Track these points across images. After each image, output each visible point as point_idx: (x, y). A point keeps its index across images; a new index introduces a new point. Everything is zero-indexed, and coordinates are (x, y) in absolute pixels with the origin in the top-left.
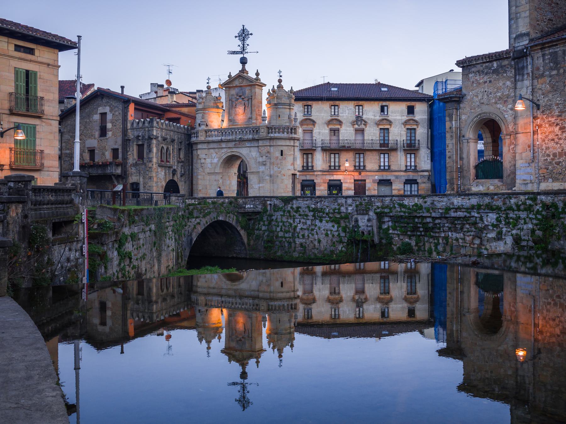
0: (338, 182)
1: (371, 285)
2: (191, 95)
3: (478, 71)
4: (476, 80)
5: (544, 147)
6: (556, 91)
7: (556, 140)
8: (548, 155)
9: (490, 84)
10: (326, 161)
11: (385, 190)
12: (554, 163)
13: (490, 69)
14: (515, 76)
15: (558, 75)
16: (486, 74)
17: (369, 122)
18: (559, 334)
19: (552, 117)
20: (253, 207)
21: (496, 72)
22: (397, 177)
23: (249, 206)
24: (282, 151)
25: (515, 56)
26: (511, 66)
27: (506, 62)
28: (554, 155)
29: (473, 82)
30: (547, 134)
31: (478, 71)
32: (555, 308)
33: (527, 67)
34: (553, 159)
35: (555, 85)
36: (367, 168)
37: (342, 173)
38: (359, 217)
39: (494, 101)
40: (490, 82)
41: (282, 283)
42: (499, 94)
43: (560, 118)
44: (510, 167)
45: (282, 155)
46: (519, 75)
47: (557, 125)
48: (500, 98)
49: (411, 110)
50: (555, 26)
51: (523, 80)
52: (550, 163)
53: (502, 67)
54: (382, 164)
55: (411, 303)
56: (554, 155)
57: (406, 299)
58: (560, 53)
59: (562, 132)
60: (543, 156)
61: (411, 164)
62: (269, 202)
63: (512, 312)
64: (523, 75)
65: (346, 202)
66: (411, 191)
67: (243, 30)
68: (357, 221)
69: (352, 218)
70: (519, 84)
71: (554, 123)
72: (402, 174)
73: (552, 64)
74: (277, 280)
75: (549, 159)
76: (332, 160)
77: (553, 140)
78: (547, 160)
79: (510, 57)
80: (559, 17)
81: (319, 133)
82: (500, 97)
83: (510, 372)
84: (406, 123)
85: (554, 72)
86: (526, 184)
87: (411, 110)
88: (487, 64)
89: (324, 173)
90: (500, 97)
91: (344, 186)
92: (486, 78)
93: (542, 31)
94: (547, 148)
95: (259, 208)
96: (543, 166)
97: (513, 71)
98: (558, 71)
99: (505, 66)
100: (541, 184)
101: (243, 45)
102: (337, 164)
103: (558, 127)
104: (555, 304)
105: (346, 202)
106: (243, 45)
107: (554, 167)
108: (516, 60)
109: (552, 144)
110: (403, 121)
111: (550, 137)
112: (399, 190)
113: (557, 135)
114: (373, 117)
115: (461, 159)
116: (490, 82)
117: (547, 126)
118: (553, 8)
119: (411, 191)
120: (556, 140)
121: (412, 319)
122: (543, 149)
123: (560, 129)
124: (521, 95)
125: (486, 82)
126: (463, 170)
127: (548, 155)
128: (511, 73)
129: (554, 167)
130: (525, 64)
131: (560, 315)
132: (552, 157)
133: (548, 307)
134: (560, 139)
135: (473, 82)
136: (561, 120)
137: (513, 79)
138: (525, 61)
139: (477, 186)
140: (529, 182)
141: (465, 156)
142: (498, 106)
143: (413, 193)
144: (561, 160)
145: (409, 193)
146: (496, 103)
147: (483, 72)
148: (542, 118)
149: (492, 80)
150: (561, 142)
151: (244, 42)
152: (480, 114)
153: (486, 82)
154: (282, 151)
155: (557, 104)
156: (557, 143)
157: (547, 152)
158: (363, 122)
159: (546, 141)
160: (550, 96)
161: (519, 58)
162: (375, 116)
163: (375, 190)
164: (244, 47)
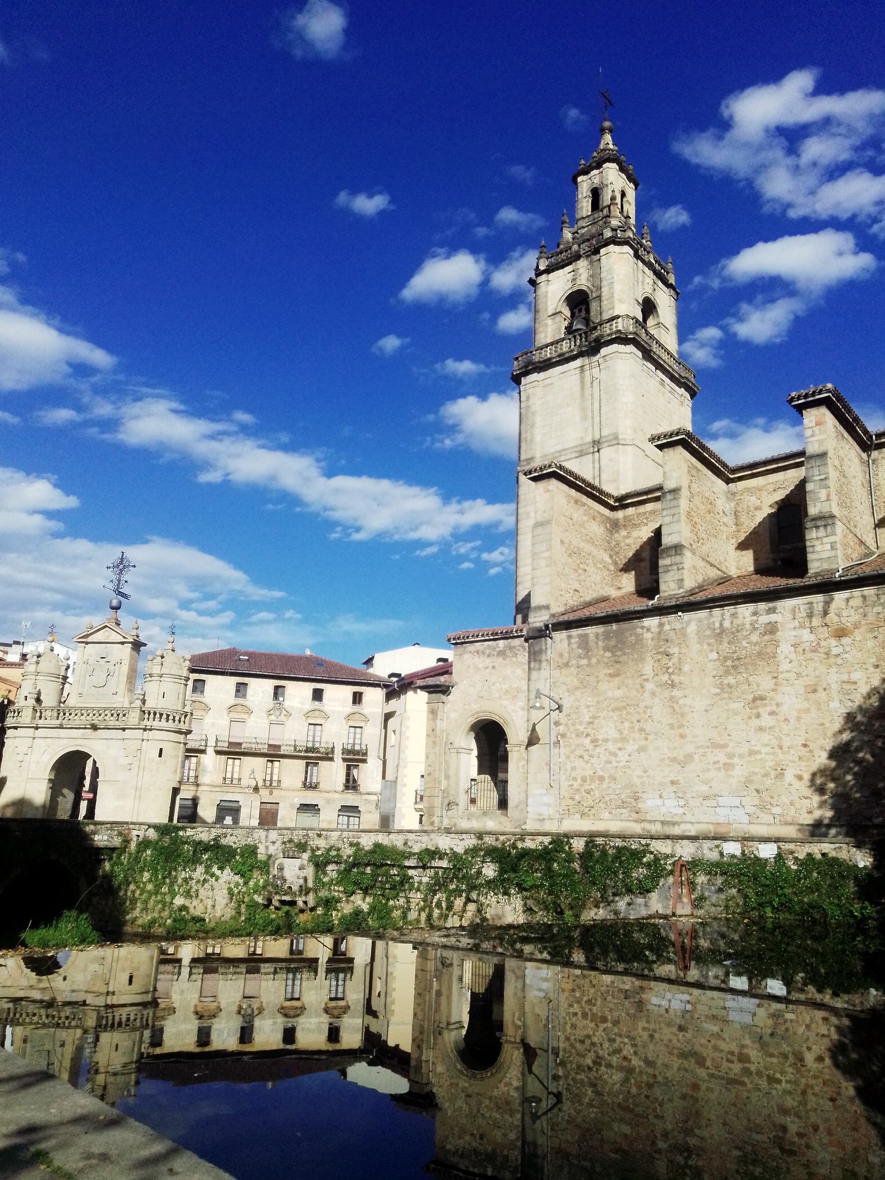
0: (234, 805)
1: (271, 982)
2: (431, 681)
3: (477, 652)
4: (474, 664)
5: (568, 767)
6: (585, 687)
7: (586, 757)
8: (575, 779)
9: (493, 671)
10: (219, 769)
11: (307, 820)
12: (582, 790)
13: (493, 649)
14: (529, 662)
15: (589, 665)
16: (489, 656)
17: (293, 712)
18: (591, 1065)
19: (581, 723)
20: (108, 840)
21: (501, 653)
22: (328, 801)
23: (100, 837)
24: (161, 750)
25: (530, 635)
26: (524, 648)
27: (517, 642)
28: (584, 780)
29: (469, 667)
30: (573, 748)
31: (477, 652)
32: (585, 1022)
33: (546, 652)
34: (581, 785)
35: (584, 679)
36: (283, 785)
37: (242, 790)
38: (287, 862)
39: (497, 695)
40: (494, 667)
41: (131, 978)
42: (506, 686)
43: (591, 726)
44: (519, 794)
45: (160, 755)
46: (535, 661)
47: (587, 735)
48: (507, 692)
49: (357, 698)
50: (582, 600)
51: (539, 669)
52: (578, 790)
53: (511, 648)
54: (229, 775)
55: (333, 1016)
56: (584, 780)
57: (326, 1010)
58: (592, 637)
59: (595, 746)
60: (567, 779)
61: (271, 777)
62: (135, 833)
63: (517, 1027)
64: (540, 661)
65: (267, 836)
66: (348, 824)
67: (122, 559)
68: (281, 869)
69: (274, 863)
70: (534, 674)
71: (583, 733)
72: (337, 796)
73: (580, 651)
74: (124, 970)
75: (576, 785)
76: (229, 769)
77: (581, 757)
78: (572, 785)
79: (522, 636)
80: (587, 588)
81: (213, 724)
82: (507, 691)
83: (512, 1136)
84: (348, 717)
85: (584, 662)
86: (542, 820)
87: (357, 698)
88: (490, 643)
89: (214, 789)
90: (507, 691)
91: (244, 813)
92: (488, 662)
93: (566, 605)
94: (574, 769)
95: (117, 842)
96: (567, 795)
97: (527, 655)
98: (589, 659)
99: (514, 647)
100: (564, 821)
101: (119, 580)
102: (236, 776)
103: (589, 738)
104: (585, 1015)
105: (267, 836)
106: (119, 580)
107: (582, 797)
108: (530, 641)
109: (579, 763)
110: (345, 715)
111: (578, 752)
112: (330, 822)
113: (587, 750)
114: (299, 706)
115: (447, 777)
116: (494, 667)
117: (573, 736)
118: (580, 575)
119: (348, 824)
120: (586, 757)
121: (289, 1047)
122: (566, 770)
123: (592, 741)
124: (538, 690)
125: (487, 667)
126: (448, 794)
127: (575, 779)
128: (523, 657)
129: (582, 797)
130: (544, 647)
131: (591, 1033)
132: (579, 781)
133: (574, 1019)
134: (591, 756)
135: (469, 667)
136: (593, 729)
137: (526, 667)
138: (544, 644)
139: (469, 819)
140: (546, 817)
141: (452, 773)
142: (504, 703)
143: (351, 827)
144: (593, 787)
145: (345, 827)
146: (500, 698)
147: (483, 653)
148: (567, 725)
149: (497, 665)
150: (593, 760)
151: (120, 577)
152: (477, 713)
153: (487, 667)
154: (161, 750)
155: (588, 707)
156: (587, 762)
157: (574, 774)
158: (284, 712)
159: (572, 758)
160: (578, 693)
161: (534, 638)
162: (302, 704)
163: (292, 820)
164: (118, 585)
